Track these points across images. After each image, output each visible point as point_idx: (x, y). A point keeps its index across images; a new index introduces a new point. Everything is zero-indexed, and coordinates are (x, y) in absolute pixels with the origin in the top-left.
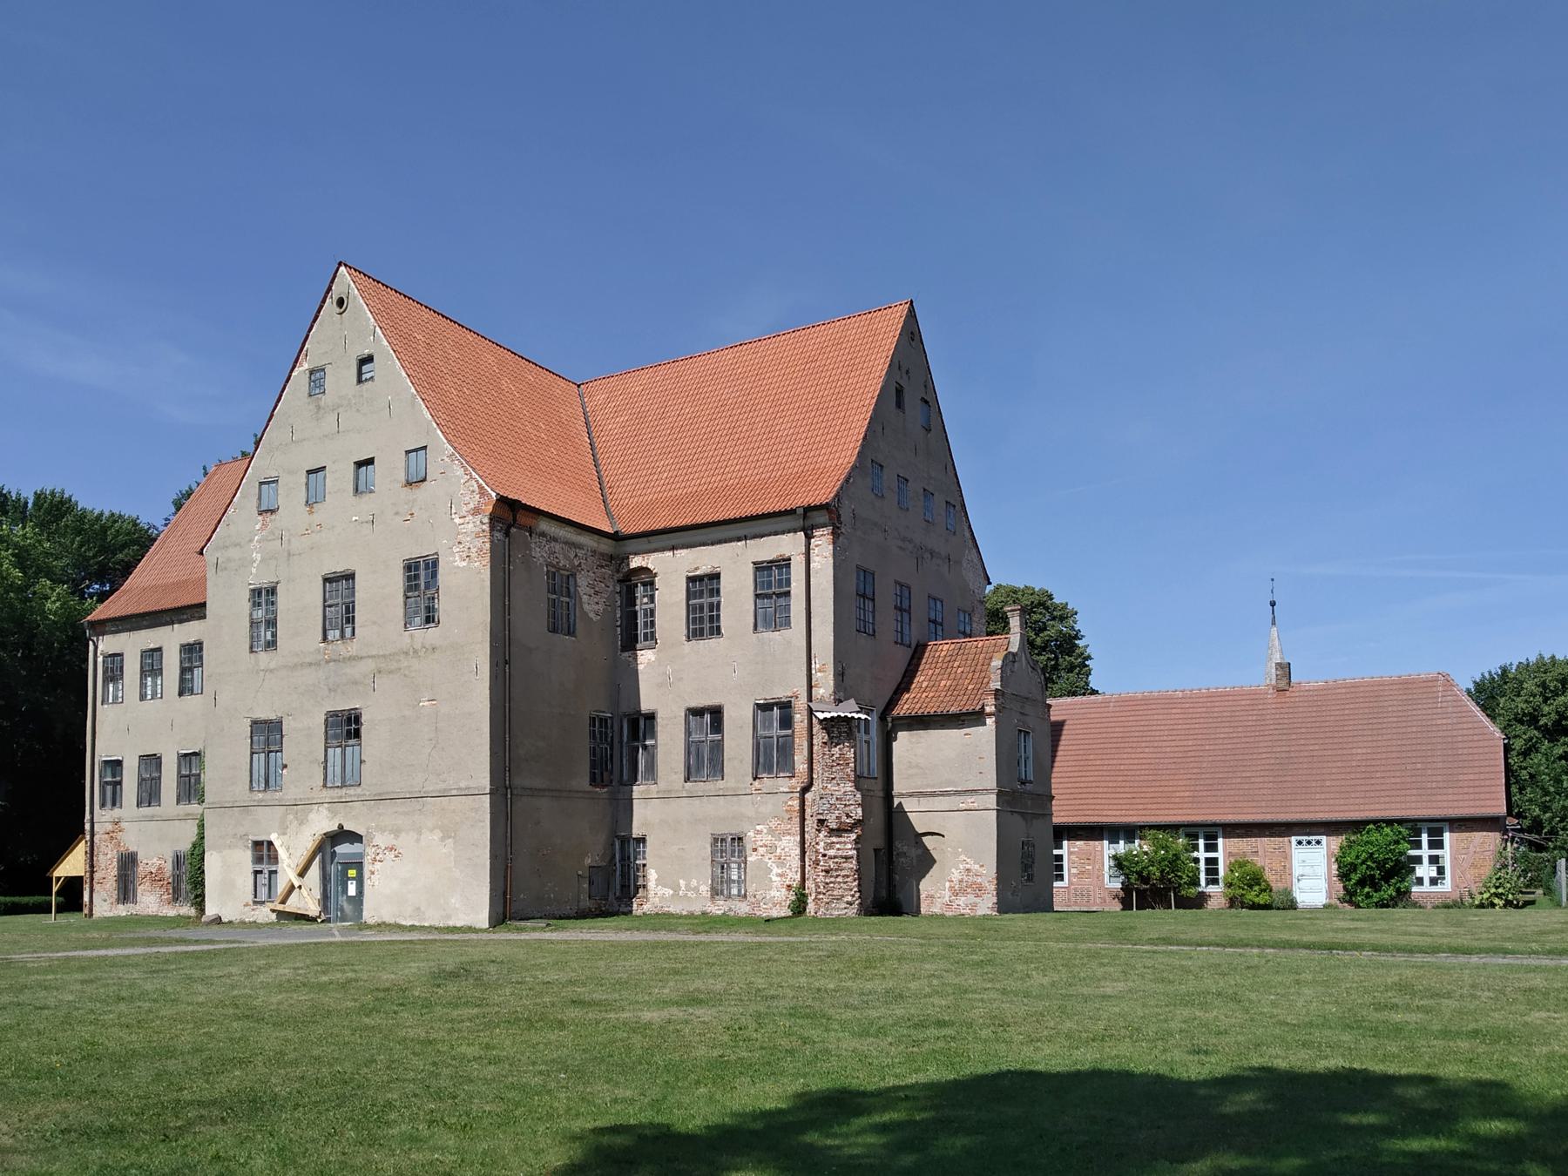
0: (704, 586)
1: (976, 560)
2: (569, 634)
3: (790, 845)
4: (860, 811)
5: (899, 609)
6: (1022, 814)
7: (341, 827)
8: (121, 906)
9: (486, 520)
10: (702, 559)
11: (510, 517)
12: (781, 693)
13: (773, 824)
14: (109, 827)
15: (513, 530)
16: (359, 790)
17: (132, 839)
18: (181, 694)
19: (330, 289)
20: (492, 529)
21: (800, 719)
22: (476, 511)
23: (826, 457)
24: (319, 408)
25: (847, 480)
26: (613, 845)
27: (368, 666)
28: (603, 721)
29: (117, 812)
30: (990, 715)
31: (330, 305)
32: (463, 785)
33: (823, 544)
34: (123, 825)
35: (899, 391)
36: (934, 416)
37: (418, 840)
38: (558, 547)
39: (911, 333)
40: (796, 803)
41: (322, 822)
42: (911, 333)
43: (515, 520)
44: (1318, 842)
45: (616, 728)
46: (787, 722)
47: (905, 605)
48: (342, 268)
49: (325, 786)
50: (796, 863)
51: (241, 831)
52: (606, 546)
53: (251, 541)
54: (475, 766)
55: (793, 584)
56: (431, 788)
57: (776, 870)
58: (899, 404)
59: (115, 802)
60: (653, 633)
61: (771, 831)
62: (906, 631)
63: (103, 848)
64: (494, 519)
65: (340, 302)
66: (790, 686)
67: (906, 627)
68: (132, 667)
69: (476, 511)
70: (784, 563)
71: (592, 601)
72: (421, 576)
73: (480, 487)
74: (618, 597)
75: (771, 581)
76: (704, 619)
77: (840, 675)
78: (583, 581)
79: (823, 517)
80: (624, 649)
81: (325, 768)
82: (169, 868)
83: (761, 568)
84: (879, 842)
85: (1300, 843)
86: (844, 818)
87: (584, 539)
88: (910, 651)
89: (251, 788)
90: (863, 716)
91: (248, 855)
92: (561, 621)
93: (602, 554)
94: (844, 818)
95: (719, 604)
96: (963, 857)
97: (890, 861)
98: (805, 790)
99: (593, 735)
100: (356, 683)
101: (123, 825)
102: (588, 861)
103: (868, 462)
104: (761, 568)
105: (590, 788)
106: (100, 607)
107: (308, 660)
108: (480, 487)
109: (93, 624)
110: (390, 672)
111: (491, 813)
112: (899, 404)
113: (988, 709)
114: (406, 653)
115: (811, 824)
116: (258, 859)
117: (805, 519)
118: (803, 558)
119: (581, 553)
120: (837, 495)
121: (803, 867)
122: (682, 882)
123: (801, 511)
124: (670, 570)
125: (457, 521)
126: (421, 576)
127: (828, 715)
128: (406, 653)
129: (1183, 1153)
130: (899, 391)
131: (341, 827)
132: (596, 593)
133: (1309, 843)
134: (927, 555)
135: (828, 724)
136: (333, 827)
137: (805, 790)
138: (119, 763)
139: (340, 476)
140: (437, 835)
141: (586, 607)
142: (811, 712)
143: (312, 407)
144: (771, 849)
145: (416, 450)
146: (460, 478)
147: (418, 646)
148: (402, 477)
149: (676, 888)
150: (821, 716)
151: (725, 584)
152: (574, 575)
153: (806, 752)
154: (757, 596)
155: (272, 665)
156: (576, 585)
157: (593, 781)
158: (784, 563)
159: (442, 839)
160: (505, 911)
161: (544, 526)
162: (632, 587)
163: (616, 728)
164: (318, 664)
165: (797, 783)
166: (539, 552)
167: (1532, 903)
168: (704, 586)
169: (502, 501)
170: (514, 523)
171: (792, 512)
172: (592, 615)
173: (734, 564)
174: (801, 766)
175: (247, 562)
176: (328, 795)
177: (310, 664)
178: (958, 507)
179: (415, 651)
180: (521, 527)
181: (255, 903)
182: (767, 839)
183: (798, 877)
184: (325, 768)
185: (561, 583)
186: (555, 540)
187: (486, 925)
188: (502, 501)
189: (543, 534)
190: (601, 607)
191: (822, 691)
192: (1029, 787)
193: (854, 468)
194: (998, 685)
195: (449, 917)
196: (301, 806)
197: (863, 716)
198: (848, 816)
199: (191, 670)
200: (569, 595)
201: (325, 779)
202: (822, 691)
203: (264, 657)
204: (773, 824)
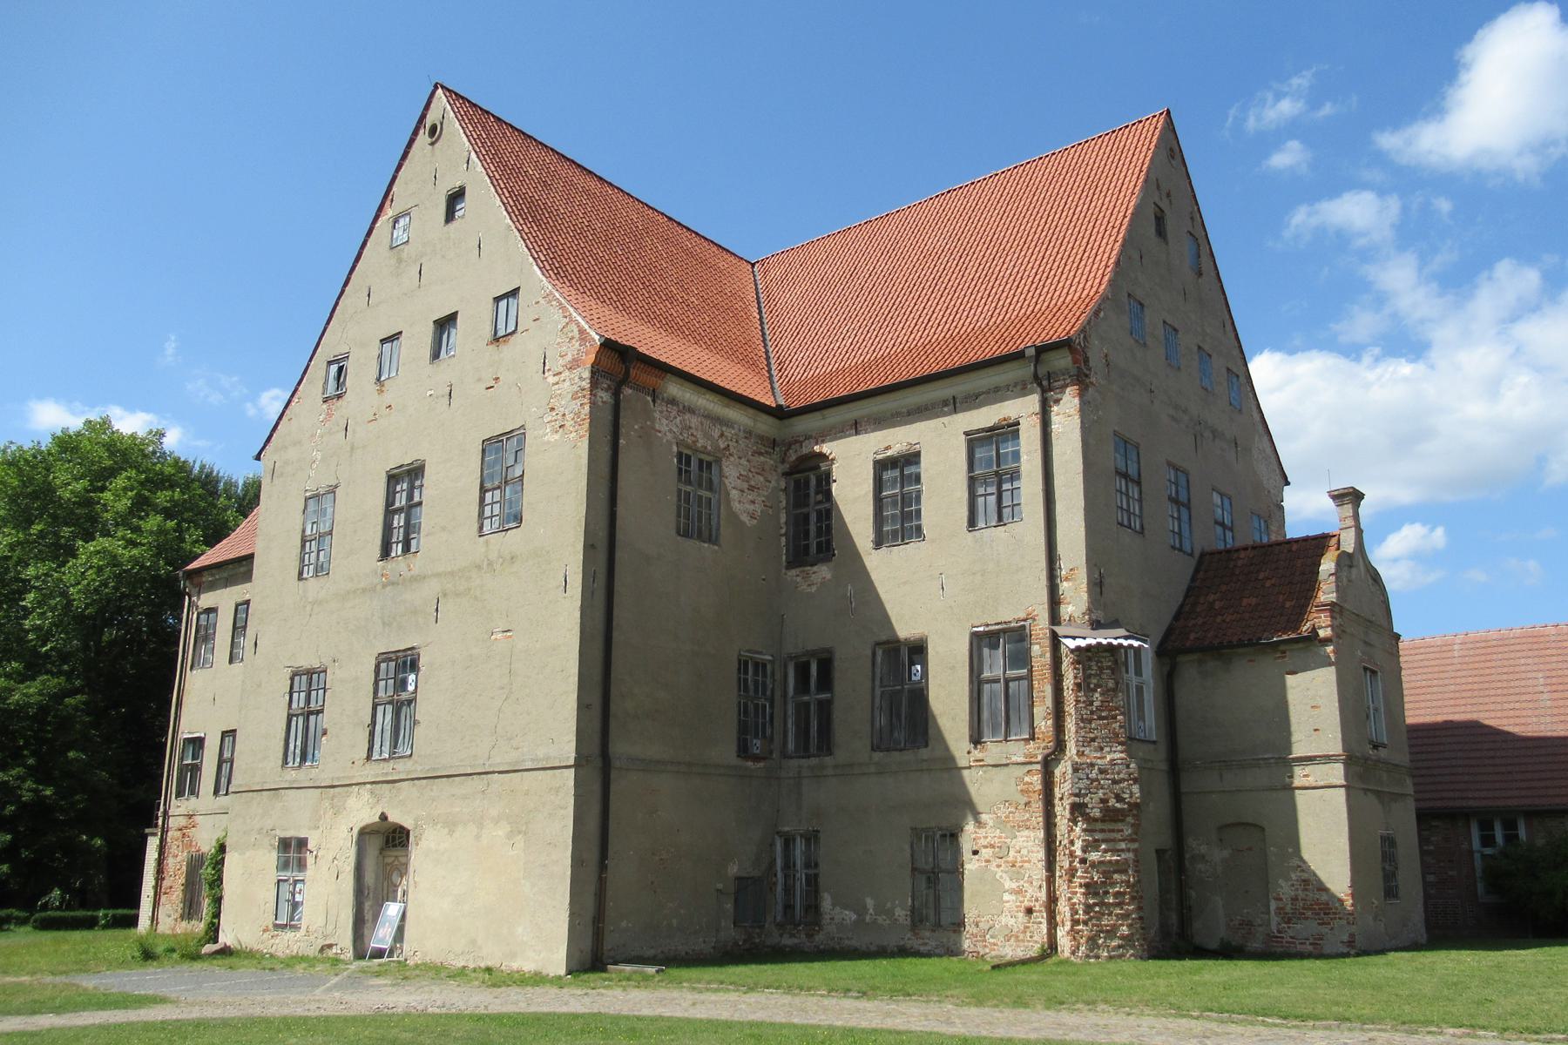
0: (898, 470)
1: (1269, 450)
2: (710, 541)
3: (1030, 844)
4: (1136, 789)
5: (1175, 501)
6: (1378, 793)
7: (383, 817)
8: (184, 924)
9: (587, 374)
11: (620, 371)
12: (1008, 614)
14: (183, 821)
15: (627, 391)
16: (409, 764)
18: (231, 662)
19: (423, 117)
20: (594, 383)
21: (1040, 652)
22: (574, 365)
23: (1069, 277)
24: (400, 261)
25: (1096, 313)
26: (772, 845)
27: (430, 589)
28: (760, 666)
30: (1326, 641)
31: (423, 138)
32: (541, 753)
33: (1067, 413)
34: (198, 819)
35: (1160, 219)
36: (1205, 258)
37: (478, 837)
38: (694, 421)
39: (1170, 149)
40: (1036, 780)
41: (362, 811)
42: (1170, 149)
43: (627, 373)
45: (778, 676)
46: (1021, 658)
47: (1183, 497)
48: (440, 91)
49: (369, 757)
50: (1040, 873)
52: (765, 425)
54: (556, 729)
55: (1024, 458)
56: (500, 760)
57: (1008, 884)
58: (1161, 232)
59: (194, 792)
60: (829, 543)
62: (1186, 533)
63: (174, 850)
64: (597, 373)
65: (433, 130)
66: (1023, 601)
67: (1185, 527)
70: (1009, 430)
71: (746, 493)
72: (500, 458)
73: (582, 331)
74: (783, 497)
75: (990, 460)
76: (899, 518)
77: (1097, 585)
78: (732, 472)
79: (1062, 361)
80: (791, 565)
81: (372, 734)
83: (975, 441)
84: (1165, 839)
86: (1112, 802)
87: (734, 414)
88: (1193, 562)
89: (285, 762)
90: (1136, 644)
91: (272, 857)
92: (696, 522)
93: (761, 438)
94: (1112, 802)
95: (919, 493)
97: (1181, 868)
99: (743, 685)
102: (733, 870)
103: (1124, 295)
104: (975, 441)
105: (739, 762)
106: (210, 552)
108: (582, 331)
109: (191, 575)
110: (458, 595)
111: (577, 796)
112: (1161, 232)
113: (1322, 633)
114: (479, 567)
115: (1062, 811)
116: (284, 865)
117: (1043, 367)
118: (1036, 421)
119: (729, 432)
120: (1083, 330)
121: (1050, 880)
122: (870, 902)
123: (1031, 352)
124: (851, 464)
125: (551, 380)
126: (500, 458)
127: (1082, 643)
128: (479, 567)
130: (1160, 219)
131: (383, 817)
132: (751, 488)
134: (1207, 434)
135: (1084, 656)
139: (419, 337)
140: (501, 831)
141: (736, 506)
142: (1055, 641)
143: (393, 261)
144: (1001, 851)
147: (493, 556)
148: (488, 333)
149: (861, 911)
150: (1072, 644)
151: (926, 467)
152: (718, 461)
153: (1049, 702)
156: (721, 475)
157: (743, 750)
158: (1009, 430)
159: (510, 835)
160: (593, 955)
161: (674, 389)
162: (808, 482)
163: (778, 676)
164: (373, 589)
165: (1038, 750)
166: (666, 426)
167: (285, 762)
168: (898, 470)
169: (608, 346)
170: (624, 381)
171: (1018, 356)
172: (745, 518)
173: (940, 444)
174: (1044, 725)
176: (373, 772)
177: (364, 590)
178: (1242, 379)
179: (490, 564)
180: (640, 388)
181: (277, 926)
183: (1043, 895)
184: (372, 734)
185: (696, 468)
186: (691, 410)
187: (562, 971)
188: (608, 346)
189: (673, 401)
190: (758, 508)
191: (1070, 609)
192: (1383, 753)
193: (1104, 299)
194: (1332, 597)
195: (513, 956)
197: (1136, 644)
198: (1119, 798)
200: (710, 488)
201: (370, 749)
202: (1070, 609)
203: (313, 586)
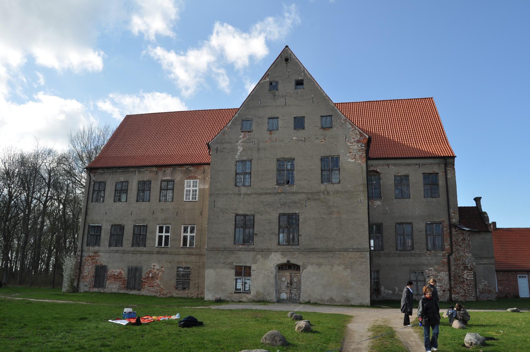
7: (288, 261)
10: (146, 176)
13: (436, 267)
17: (103, 259)
27: (304, 196)
29: (96, 248)
37: (331, 269)
44: (525, 277)
51: (230, 261)
53: (237, 142)
61: (435, 270)
68: (155, 187)
69: (358, 142)
73: (360, 133)
82: (124, 274)
85: (520, 277)
96: (483, 281)
98: (450, 255)
100: (296, 203)
101: (101, 254)
107: (269, 192)
108: (360, 133)
122: (397, 288)
125: (349, 144)
129: (241, 350)
133: (522, 277)
136: (284, 261)
137: (450, 255)
138: (100, 228)
145: (326, 116)
146: (350, 129)
154: (424, 184)
155: (248, 192)
159: (345, 269)
175: (235, 150)
182: (434, 273)
191: (454, 220)
196: (266, 252)
199: (143, 191)
202: (454, 220)
204: (436, 267)
